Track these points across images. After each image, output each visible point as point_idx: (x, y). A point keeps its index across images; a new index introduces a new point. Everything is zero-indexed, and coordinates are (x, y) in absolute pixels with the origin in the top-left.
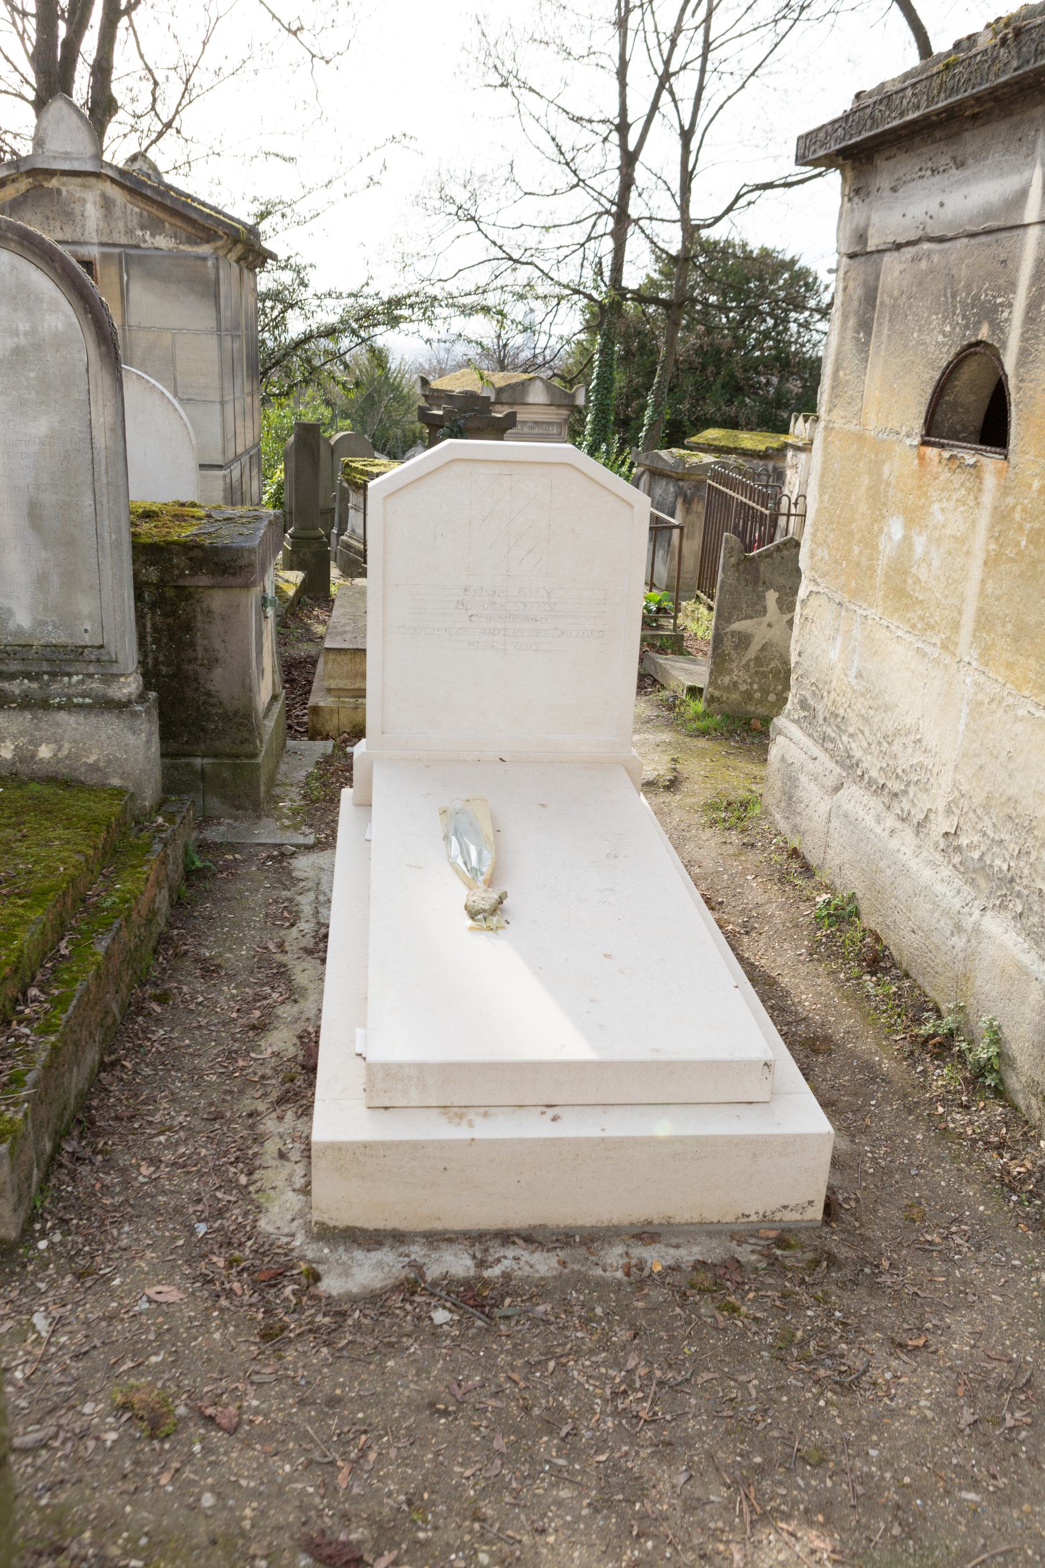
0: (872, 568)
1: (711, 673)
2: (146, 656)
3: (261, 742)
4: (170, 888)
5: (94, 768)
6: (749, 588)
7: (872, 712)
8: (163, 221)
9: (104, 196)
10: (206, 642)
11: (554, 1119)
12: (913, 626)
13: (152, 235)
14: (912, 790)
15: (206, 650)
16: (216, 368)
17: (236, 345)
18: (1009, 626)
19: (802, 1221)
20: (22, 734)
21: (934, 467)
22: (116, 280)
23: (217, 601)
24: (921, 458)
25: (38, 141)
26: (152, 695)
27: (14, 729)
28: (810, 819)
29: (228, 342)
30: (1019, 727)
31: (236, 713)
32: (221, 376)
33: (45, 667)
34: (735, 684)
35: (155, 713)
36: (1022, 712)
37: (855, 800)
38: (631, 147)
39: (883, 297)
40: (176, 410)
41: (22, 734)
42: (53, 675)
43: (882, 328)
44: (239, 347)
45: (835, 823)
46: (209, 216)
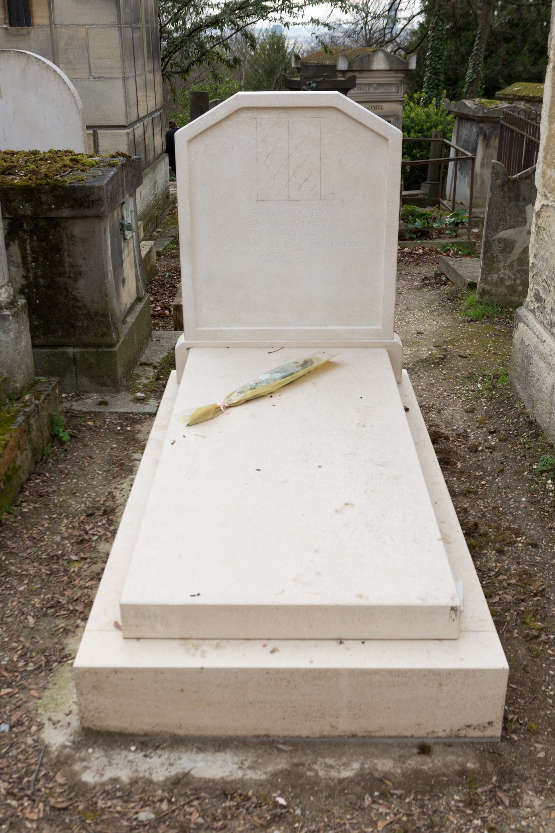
1: (483, 272)
2: (28, 272)
3: (118, 335)
6: (512, 204)
10: (71, 260)
11: (273, 652)
15: (72, 266)
16: (118, 52)
19: (484, 737)
23: (78, 228)
28: (540, 390)
29: (128, 33)
31: (97, 314)
34: (502, 280)
35: (25, 316)
40: (65, 83)
44: (141, 36)
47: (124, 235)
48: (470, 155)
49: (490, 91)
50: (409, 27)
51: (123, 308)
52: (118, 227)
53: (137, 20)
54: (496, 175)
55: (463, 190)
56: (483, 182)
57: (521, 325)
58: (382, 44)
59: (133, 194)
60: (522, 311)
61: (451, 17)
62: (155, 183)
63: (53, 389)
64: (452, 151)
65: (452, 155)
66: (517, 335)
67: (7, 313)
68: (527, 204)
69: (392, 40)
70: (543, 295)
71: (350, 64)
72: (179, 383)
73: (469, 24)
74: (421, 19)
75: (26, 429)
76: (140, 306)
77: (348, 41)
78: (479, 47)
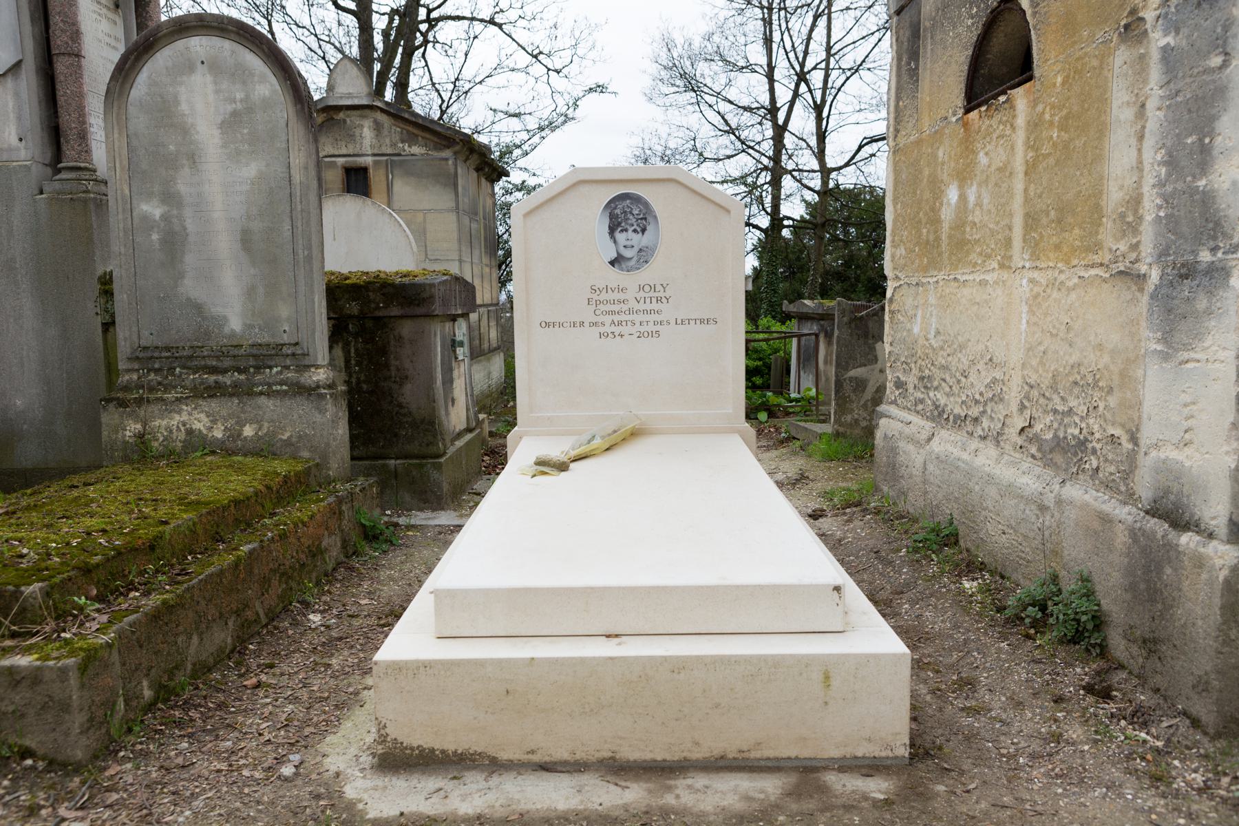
0: (938, 239)
2: (350, 376)
5: (288, 443)
6: (861, 341)
7: (950, 359)
8: (417, 136)
9: (376, 122)
10: (397, 363)
15: (398, 370)
16: (455, 235)
18: (1053, 213)
20: (231, 416)
22: (384, 178)
23: (406, 329)
24: (966, 125)
25: (330, 88)
27: (224, 413)
29: (466, 220)
31: (422, 421)
32: (459, 241)
33: (252, 362)
34: (856, 421)
37: (947, 443)
38: (781, 122)
41: (231, 416)
42: (258, 368)
45: (931, 467)
47: (455, 351)
56: (827, 380)
62: (490, 373)
68: (877, 341)
76: (469, 436)
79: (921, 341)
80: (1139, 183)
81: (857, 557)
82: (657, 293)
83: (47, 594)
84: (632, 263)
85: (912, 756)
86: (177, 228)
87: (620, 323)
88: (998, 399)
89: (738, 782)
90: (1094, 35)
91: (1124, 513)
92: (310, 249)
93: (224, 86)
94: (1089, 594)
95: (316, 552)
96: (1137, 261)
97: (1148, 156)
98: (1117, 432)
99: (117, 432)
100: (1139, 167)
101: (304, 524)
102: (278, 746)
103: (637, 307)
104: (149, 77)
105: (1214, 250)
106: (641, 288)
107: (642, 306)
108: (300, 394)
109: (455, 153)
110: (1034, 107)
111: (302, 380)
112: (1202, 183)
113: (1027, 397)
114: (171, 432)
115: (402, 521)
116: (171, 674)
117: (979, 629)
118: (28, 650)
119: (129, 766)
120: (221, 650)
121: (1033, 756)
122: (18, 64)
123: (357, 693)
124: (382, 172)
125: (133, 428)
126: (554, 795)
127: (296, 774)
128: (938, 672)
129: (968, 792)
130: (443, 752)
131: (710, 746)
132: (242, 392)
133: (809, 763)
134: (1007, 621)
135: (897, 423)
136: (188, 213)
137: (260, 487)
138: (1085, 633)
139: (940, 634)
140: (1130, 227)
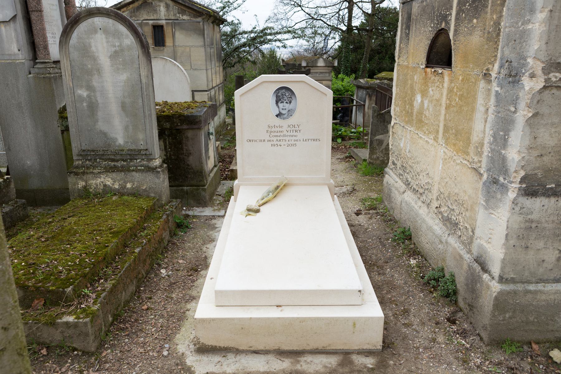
0: (412, 113)
2: (167, 153)
3: (207, 181)
4: (170, 231)
5: (145, 190)
6: (382, 124)
12: (425, 133)
13: (182, 16)
14: (426, 192)
15: (187, 150)
16: (204, 58)
17: (212, 50)
21: (430, 75)
22: (171, 31)
23: (190, 134)
24: (426, 72)
26: (165, 165)
28: (396, 204)
29: (208, 50)
30: (458, 167)
31: (197, 171)
32: (206, 60)
33: (128, 157)
34: (378, 158)
35: (166, 172)
36: (459, 162)
37: (409, 197)
39: (413, 17)
42: (131, 160)
43: (413, 28)
44: (214, 51)
46: (200, 8)
48: (363, 103)
49: (371, 76)
50: (334, 47)
51: (209, 169)
52: (207, 134)
53: (212, 44)
54: (374, 111)
55: (360, 119)
56: (369, 116)
57: (386, 176)
58: (322, 55)
59: (213, 120)
60: (387, 170)
61: (353, 43)
63: (179, 204)
64: (355, 102)
65: (355, 103)
66: (385, 182)
67: (159, 170)
69: (326, 53)
70: (396, 162)
71: (307, 64)
72: (236, 201)
73: (361, 46)
74: (339, 44)
75: (167, 221)
76: (216, 169)
77: (306, 54)
78: (366, 55)
79: (403, 151)
80: (484, 137)
81: (372, 240)
82: (296, 129)
83: (74, 290)
84: (285, 116)
85: (383, 347)
86: (94, 101)
87: (280, 140)
88: (429, 190)
89: (322, 359)
90: (474, 69)
91: (467, 256)
92: (151, 111)
93: (111, 39)
94: (453, 281)
95: (161, 241)
96: (480, 167)
97: (487, 130)
98: (468, 227)
99: (75, 185)
100: (484, 132)
101: (156, 232)
102: (161, 340)
103: (287, 134)
104: (78, 35)
105: (505, 179)
106: (289, 126)
107: (289, 134)
108: (149, 171)
109: (203, 19)
110: (451, 83)
111: (150, 165)
112: (503, 152)
113: (439, 195)
114: (97, 185)
115: (190, 213)
116: (117, 309)
117: (413, 286)
118: (70, 314)
119: (109, 351)
120: (132, 293)
121: (425, 348)
122: (14, 17)
123: (184, 313)
124: (170, 28)
125: (81, 184)
126: (258, 363)
127: (169, 354)
128: (397, 305)
129: (400, 364)
130: (220, 347)
131: (313, 345)
132: (126, 170)
133: (347, 351)
134: (424, 284)
135: (391, 178)
136: (98, 94)
137: (139, 218)
138: (450, 295)
139: (399, 287)
140: (480, 154)
